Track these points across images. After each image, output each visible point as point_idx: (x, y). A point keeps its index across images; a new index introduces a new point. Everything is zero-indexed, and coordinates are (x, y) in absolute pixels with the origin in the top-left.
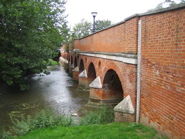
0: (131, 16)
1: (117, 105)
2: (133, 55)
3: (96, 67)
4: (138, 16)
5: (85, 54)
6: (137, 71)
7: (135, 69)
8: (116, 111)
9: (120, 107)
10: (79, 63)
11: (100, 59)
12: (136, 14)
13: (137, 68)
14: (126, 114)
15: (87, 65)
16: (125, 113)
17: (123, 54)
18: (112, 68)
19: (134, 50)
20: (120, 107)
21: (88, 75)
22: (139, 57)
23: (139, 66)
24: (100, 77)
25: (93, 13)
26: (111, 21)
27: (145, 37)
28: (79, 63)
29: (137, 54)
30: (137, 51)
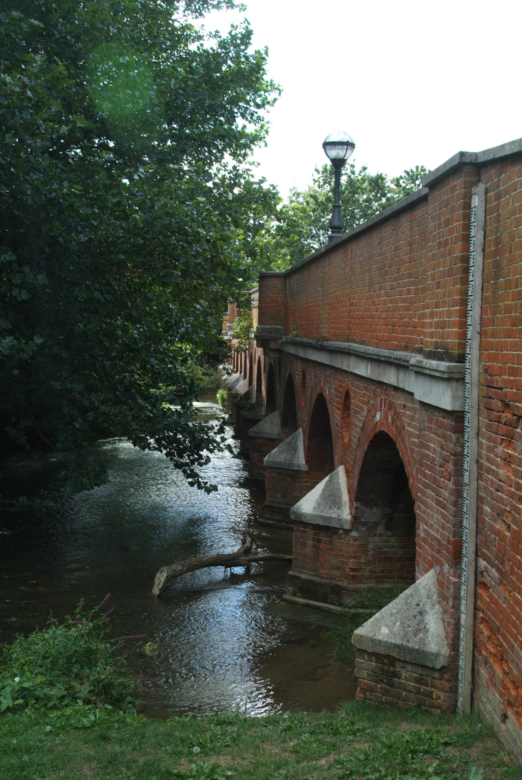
0: (445, 164)
1: (371, 615)
2: (443, 365)
3: (336, 416)
4: (470, 164)
5: (301, 353)
6: (463, 447)
7: (454, 437)
8: (362, 652)
9: (385, 630)
10: (304, 414)
11: (348, 381)
12: (462, 154)
13: (459, 429)
14: (410, 667)
15: (351, 438)
16: (404, 661)
17: (415, 359)
18: (392, 433)
19: (453, 341)
20: (385, 630)
21: (307, 462)
22: (473, 369)
23: (471, 421)
24: (347, 472)
25: (327, 145)
26: (271, 72)
27: (494, 273)
28: (304, 414)
29: (462, 359)
30: (463, 346)
